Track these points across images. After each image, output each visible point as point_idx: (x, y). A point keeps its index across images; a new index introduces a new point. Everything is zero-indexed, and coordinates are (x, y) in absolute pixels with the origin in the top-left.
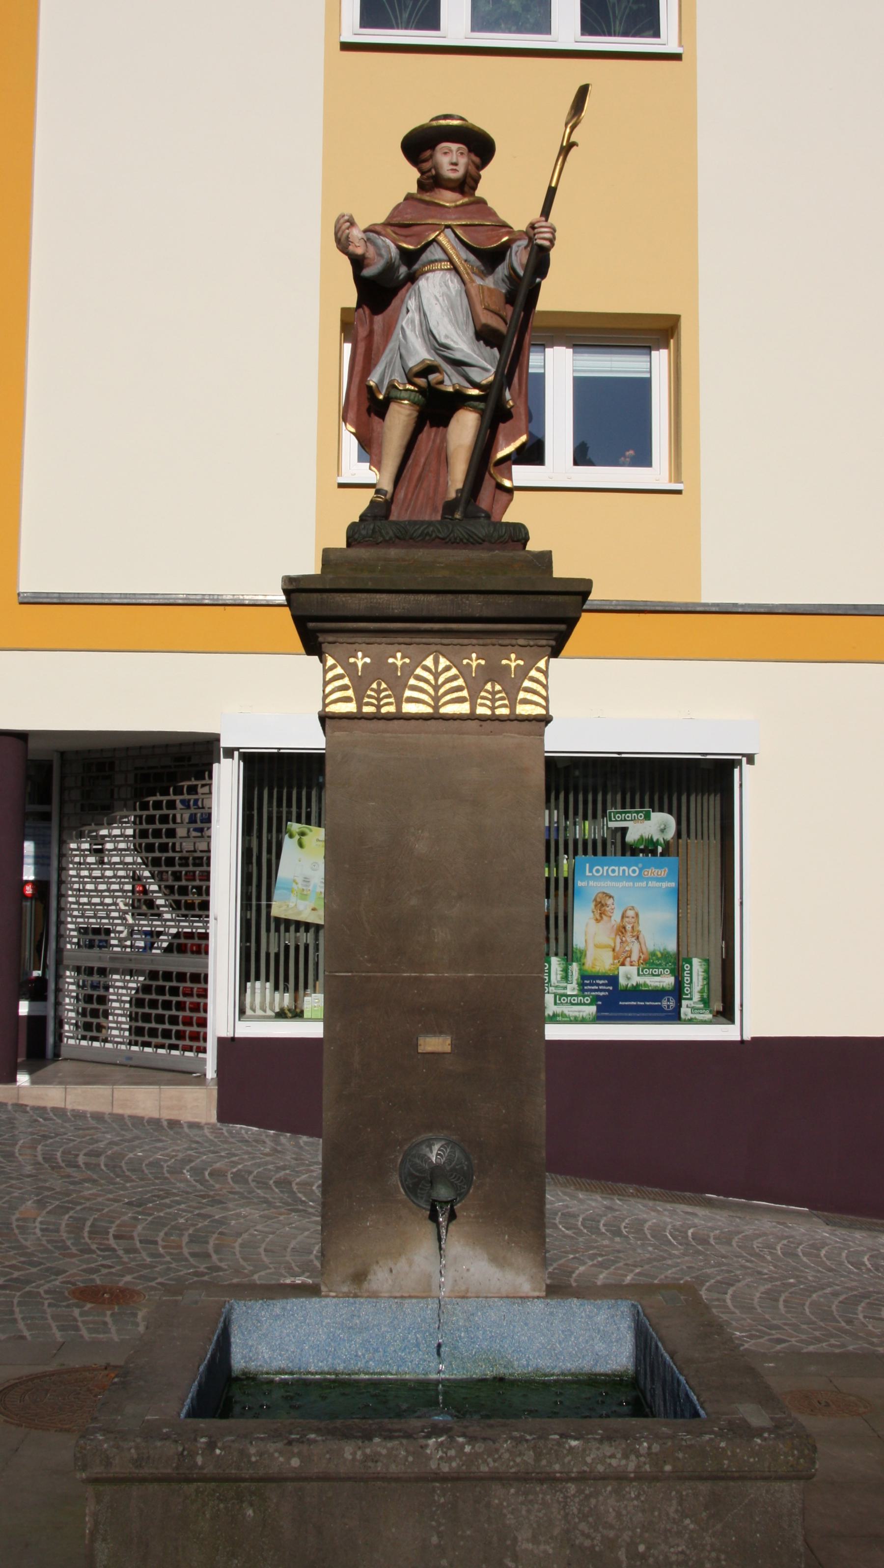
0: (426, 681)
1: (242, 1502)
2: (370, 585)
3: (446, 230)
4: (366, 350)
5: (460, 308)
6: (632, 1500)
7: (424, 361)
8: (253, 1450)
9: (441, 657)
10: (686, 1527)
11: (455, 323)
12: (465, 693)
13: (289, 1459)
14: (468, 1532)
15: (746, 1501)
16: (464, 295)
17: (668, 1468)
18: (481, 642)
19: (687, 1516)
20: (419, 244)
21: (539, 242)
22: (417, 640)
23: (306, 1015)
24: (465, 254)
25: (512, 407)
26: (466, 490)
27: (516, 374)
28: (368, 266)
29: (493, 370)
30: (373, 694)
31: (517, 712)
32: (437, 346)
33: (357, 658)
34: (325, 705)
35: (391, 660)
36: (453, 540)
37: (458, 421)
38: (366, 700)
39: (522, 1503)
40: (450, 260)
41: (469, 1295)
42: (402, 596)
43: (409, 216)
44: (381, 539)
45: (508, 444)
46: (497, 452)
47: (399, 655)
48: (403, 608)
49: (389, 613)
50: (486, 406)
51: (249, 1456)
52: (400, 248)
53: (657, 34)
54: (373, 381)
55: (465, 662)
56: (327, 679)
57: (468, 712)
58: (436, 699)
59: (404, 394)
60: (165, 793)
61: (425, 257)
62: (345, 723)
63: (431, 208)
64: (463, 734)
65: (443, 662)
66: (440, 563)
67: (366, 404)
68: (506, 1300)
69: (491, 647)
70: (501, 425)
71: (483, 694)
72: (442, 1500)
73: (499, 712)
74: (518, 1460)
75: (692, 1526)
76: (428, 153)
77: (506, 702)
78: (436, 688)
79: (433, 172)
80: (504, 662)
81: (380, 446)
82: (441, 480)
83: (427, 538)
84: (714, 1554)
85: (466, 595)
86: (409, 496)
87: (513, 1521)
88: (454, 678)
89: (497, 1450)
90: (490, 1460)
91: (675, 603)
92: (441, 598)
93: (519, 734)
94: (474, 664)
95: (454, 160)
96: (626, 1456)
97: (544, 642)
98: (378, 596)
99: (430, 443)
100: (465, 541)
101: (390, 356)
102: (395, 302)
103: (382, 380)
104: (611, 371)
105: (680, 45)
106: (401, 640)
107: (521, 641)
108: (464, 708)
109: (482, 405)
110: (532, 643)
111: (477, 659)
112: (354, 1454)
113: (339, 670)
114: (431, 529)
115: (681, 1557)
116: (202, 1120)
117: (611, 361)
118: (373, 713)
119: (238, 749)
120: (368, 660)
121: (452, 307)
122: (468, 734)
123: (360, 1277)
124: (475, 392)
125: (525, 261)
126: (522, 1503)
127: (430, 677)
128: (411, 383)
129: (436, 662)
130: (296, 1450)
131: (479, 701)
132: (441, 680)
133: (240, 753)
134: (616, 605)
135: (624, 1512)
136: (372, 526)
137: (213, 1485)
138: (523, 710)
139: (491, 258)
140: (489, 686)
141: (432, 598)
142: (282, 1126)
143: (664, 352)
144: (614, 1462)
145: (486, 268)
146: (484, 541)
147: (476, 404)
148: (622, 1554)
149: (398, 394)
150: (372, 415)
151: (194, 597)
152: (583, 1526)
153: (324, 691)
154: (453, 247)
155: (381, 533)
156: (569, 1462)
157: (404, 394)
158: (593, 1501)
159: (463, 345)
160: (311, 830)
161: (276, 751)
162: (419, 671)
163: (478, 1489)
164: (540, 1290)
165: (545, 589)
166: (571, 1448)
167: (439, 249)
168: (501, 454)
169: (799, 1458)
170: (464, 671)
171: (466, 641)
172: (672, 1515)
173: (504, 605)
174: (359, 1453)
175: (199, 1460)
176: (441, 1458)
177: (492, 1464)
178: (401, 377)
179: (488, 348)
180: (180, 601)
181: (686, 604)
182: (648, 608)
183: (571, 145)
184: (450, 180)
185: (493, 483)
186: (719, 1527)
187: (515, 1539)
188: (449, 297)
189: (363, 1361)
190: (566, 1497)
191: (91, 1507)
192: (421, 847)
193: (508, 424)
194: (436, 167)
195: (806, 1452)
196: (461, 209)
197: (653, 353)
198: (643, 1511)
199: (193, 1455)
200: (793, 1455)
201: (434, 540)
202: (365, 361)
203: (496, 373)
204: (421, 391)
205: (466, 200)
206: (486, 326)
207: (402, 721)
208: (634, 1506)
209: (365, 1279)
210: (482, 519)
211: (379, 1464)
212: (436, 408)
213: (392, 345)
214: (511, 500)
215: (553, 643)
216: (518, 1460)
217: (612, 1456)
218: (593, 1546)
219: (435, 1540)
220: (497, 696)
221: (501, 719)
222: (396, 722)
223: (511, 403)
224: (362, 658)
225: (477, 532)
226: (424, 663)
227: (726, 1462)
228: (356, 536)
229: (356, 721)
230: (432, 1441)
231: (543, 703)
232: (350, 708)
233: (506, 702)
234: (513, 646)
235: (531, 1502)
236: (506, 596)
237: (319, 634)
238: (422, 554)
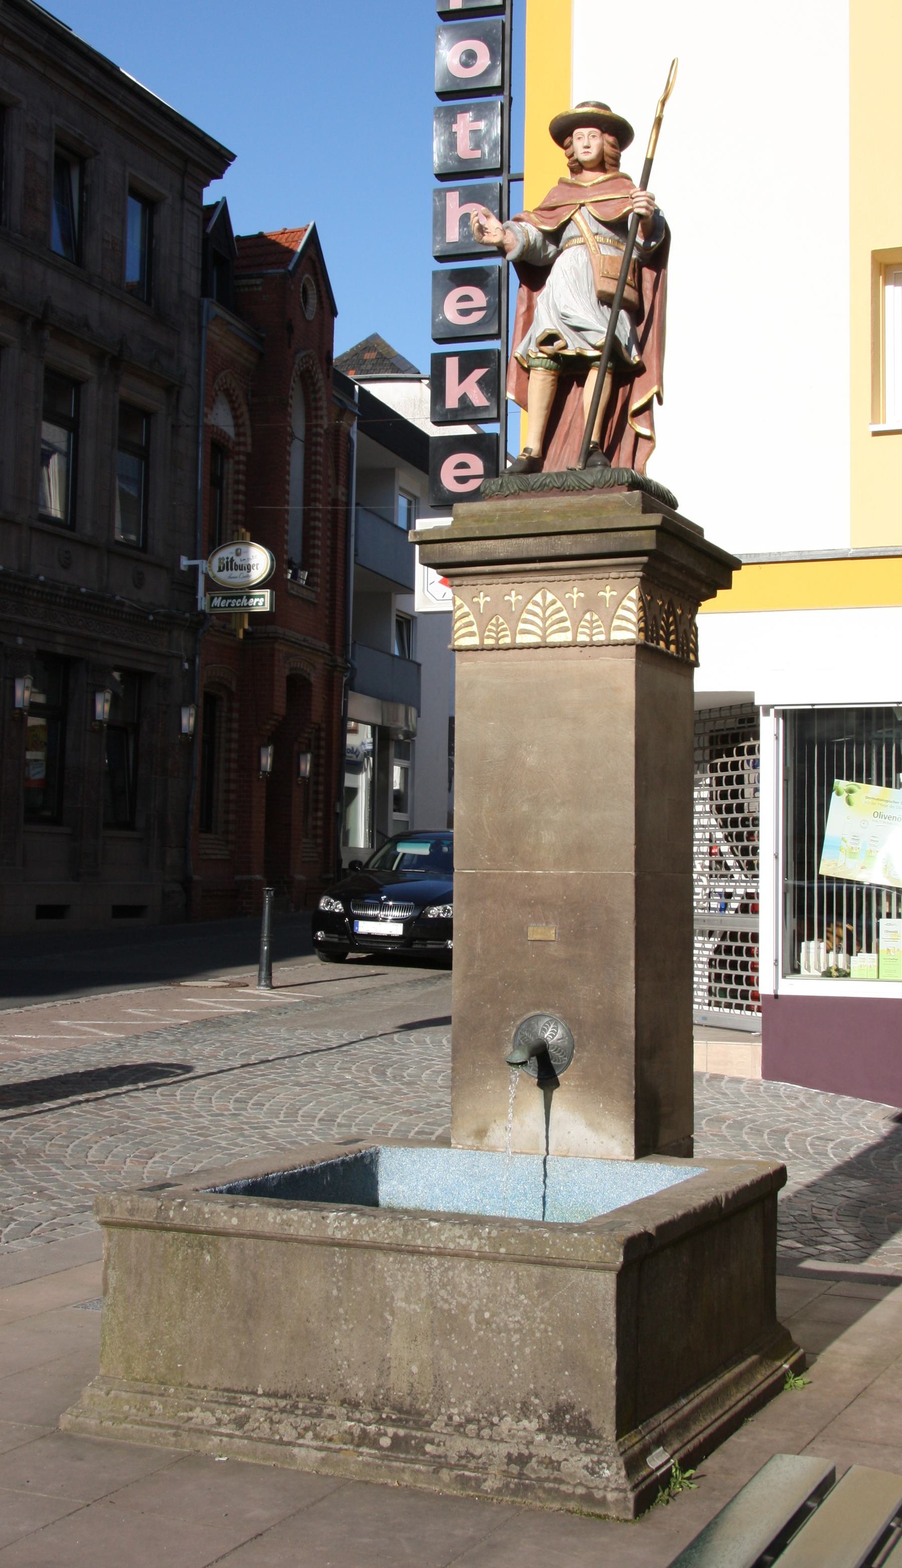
0: (535, 614)
1: (203, 1249)
2: (478, 534)
5: (585, 279)
6: (480, 1275)
8: (206, 1209)
10: (521, 1302)
13: (230, 1218)
14: (359, 1289)
15: (569, 1285)
17: (503, 1250)
18: (579, 577)
19: (522, 1293)
22: (526, 579)
23: (852, 976)
28: (509, 250)
35: (507, 598)
39: (398, 1270)
41: (569, 1154)
44: (508, 492)
45: (640, 397)
47: (513, 593)
51: (204, 1214)
52: (540, 230)
58: (544, 630)
59: (537, 362)
60: (730, 755)
62: (470, 654)
63: (573, 189)
65: (550, 597)
68: (599, 1161)
72: (340, 1262)
73: (595, 638)
74: (391, 1233)
75: (526, 1301)
84: (542, 1326)
87: (391, 1284)
88: (559, 611)
89: (376, 1224)
90: (370, 1231)
92: (538, 540)
93: (613, 657)
95: (585, 144)
96: (471, 1238)
97: (632, 574)
107: (613, 575)
112: (275, 1218)
114: (548, 480)
115: (517, 1326)
116: (747, 1076)
119: (773, 706)
122: (570, 659)
123: (481, 1133)
126: (398, 1270)
129: (544, 597)
130: (236, 1212)
133: (776, 711)
135: (474, 1285)
137: (183, 1235)
141: (531, 540)
142: (826, 1086)
144: (462, 1242)
146: (593, 487)
148: (472, 1318)
152: (443, 1293)
156: (428, 1239)
157: (537, 362)
158: (451, 1273)
160: (859, 788)
161: (810, 707)
162: (530, 606)
163: (366, 1255)
164: (629, 1155)
166: (431, 1227)
169: (606, 1252)
170: (568, 603)
171: (566, 577)
172: (510, 1290)
173: (590, 543)
174: (278, 1218)
175: (171, 1214)
176: (337, 1227)
177: (372, 1235)
186: (547, 1304)
187: (392, 1298)
189: (482, 1205)
190: (430, 1268)
191: (105, 1244)
192: (531, 761)
195: (612, 1247)
196: (597, 186)
198: (489, 1285)
199: (167, 1209)
200: (601, 1249)
205: (608, 176)
207: (516, 650)
208: (482, 1281)
209: (485, 1136)
211: (292, 1228)
214: (653, 448)
216: (391, 1233)
217: (461, 1237)
218: (450, 1310)
219: (335, 1292)
220: (595, 625)
227: (548, 1249)
230: (332, 1215)
235: (404, 1269)
236: (591, 535)
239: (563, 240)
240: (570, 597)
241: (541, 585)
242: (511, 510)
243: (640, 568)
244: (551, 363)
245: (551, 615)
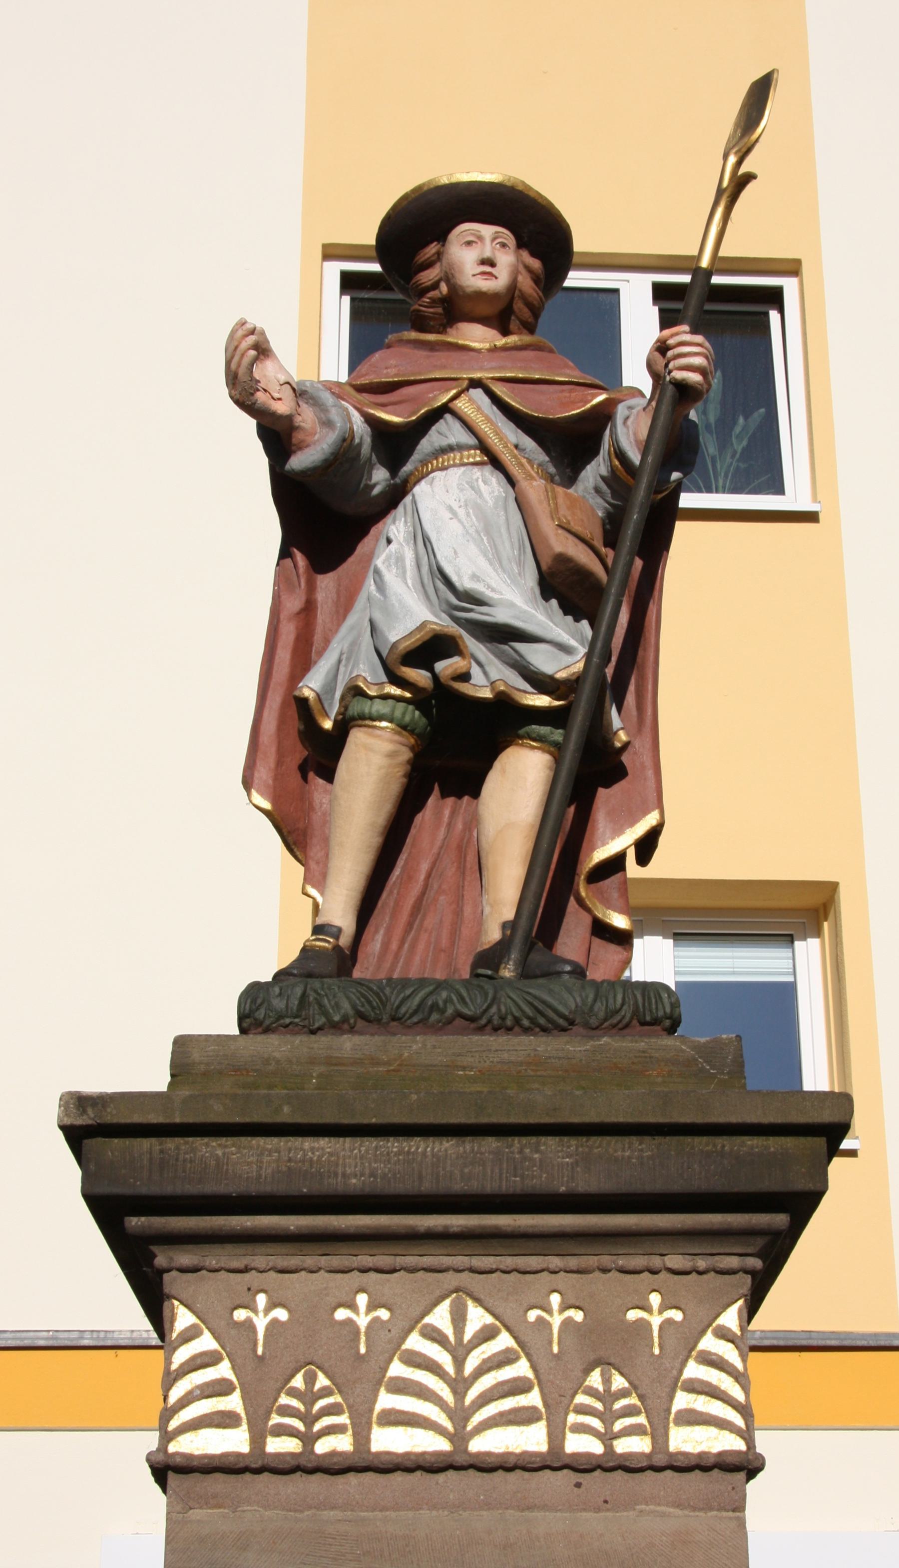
3: (472, 391)
4: (298, 639)
5: (504, 530)
7: (424, 624)
9: (470, 1303)
11: (496, 559)
12: (533, 1399)
16: (513, 506)
18: (573, 1262)
20: (414, 413)
21: (679, 375)
24: (512, 434)
25: (626, 745)
26: (523, 922)
27: (632, 688)
29: (582, 651)
30: (295, 1403)
31: (672, 1448)
32: (455, 601)
33: (255, 1311)
34: (167, 1437)
35: (341, 1314)
36: (496, 1021)
37: (504, 771)
38: (275, 1419)
40: (484, 447)
42: (370, 1144)
43: (393, 371)
44: (320, 1021)
45: (618, 832)
46: (593, 849)
47: (362, 1300)
48: (373, 1174)
49: (334, 1185)
50: (566, 737)
53: (779, 489)
54: (311, 686)
55: (533, 1315)
56: (174, 1367)
57: (543, 1447)
58: (460, 1415)
59: (379, 707)
61: (426, 444)
62: (218, 1483)
64: (530, 1508)
65: (477, 1318)
66: (464, 1068)
67: (299, 753)
69: (597, 1274)
70: (602, 792)
71: (581, 1399)
73: (623, 1446)
76: (432, 249)
77: (642, 1419)
78: (459, 1385)
79: (444, 288)
80: (633, 1315)
81: (326, 841)
82: (468, 911)
83: (435, 1017)
85: (534, 1139)
86: (394, 946)
88: (505, 1359)
91: (858, 1334)
92: (469, 1145)
93: (679, 1506)
94: (556, 1321)
95: (487, 254)
97: (733, 1262)
98: (308, 1143)
99: (442, 831)
100: (526, 1023)
101: (350, 639)
102: (362, 548)
103: (330, 686)
104: (734, 973)
105: (815, 499)
106: (366, 1260)
107: (675, 1261)
108: (532, 1439)
109: (557, 735)
110: (702, 1264)
111: (564, 1307)
113: (206, 1342)
114: (444, 994)
117: (733, 958)
118: (292, 1455)
120: (281, 1314)
121: (488, 529)
122: (544, 1507)
124: (543, 701)
125: (644, 433)
127: (445, 1360)
128: (395, 679)
129: (459, 1318)
131: (572, 1418)
132: (472, 1363)
134: (761, 1338)
136: (299, 991)
138: (685, 1440)
139: (570, 443)
140: (595, 1379)
141: (447, 1146)
143: (813, 943)
145: (560, 473)
146: (572, 1023)
147: (544, 730)
149: (366, 707)
150: (311, 775)
151: (66, 1335)
153: (165, 1398)
154: (488, 420)
155: (321, 1005)
157: (379, 707)
159: (514, 597)
165: (734, 1119)
167: (457, 426)
168: (601, 854)
170: (528, 1343)
171: (534, 1262)
178: (374, 672)
179: (570, 618)
180: (42, 1343)
181: (876, 1335)
182: (814, 1343)
183: (741, 182)
184: (480, 296)
185: (587, 920)
188: (480, 511)
193: (618, 788)
194: (448, 278)
197: (797, 943)
201: (450, 1022)
202: (295, 638)
203: (589, 656)
204: (421, 699)
206: (562, 559)
207: (369, 1476)
210: (566, 977)
212: (454, 741)
213: (357, 618)
215: (756, 1263)
220: (618, 1405)
221: (628, 1466)
222: (353, 1479)
223: (623, 736)
224: (267, 1311)
225: (555, 1003)
226: (427, 1320)
228: (260, 1014)
229: (248, 1476)
231: (739, 1421)
232: (235, 1441)
233: (642, 1419)
234: (654, 1272)
237: (154, 1249)
238: (419, 1048)
239: (416, 457)
240: (249, 1321)
241: (451, 1280)
242: (356, 1062)
243: (760, 1242)
244: (412, 714)
245: (480, 1372)
